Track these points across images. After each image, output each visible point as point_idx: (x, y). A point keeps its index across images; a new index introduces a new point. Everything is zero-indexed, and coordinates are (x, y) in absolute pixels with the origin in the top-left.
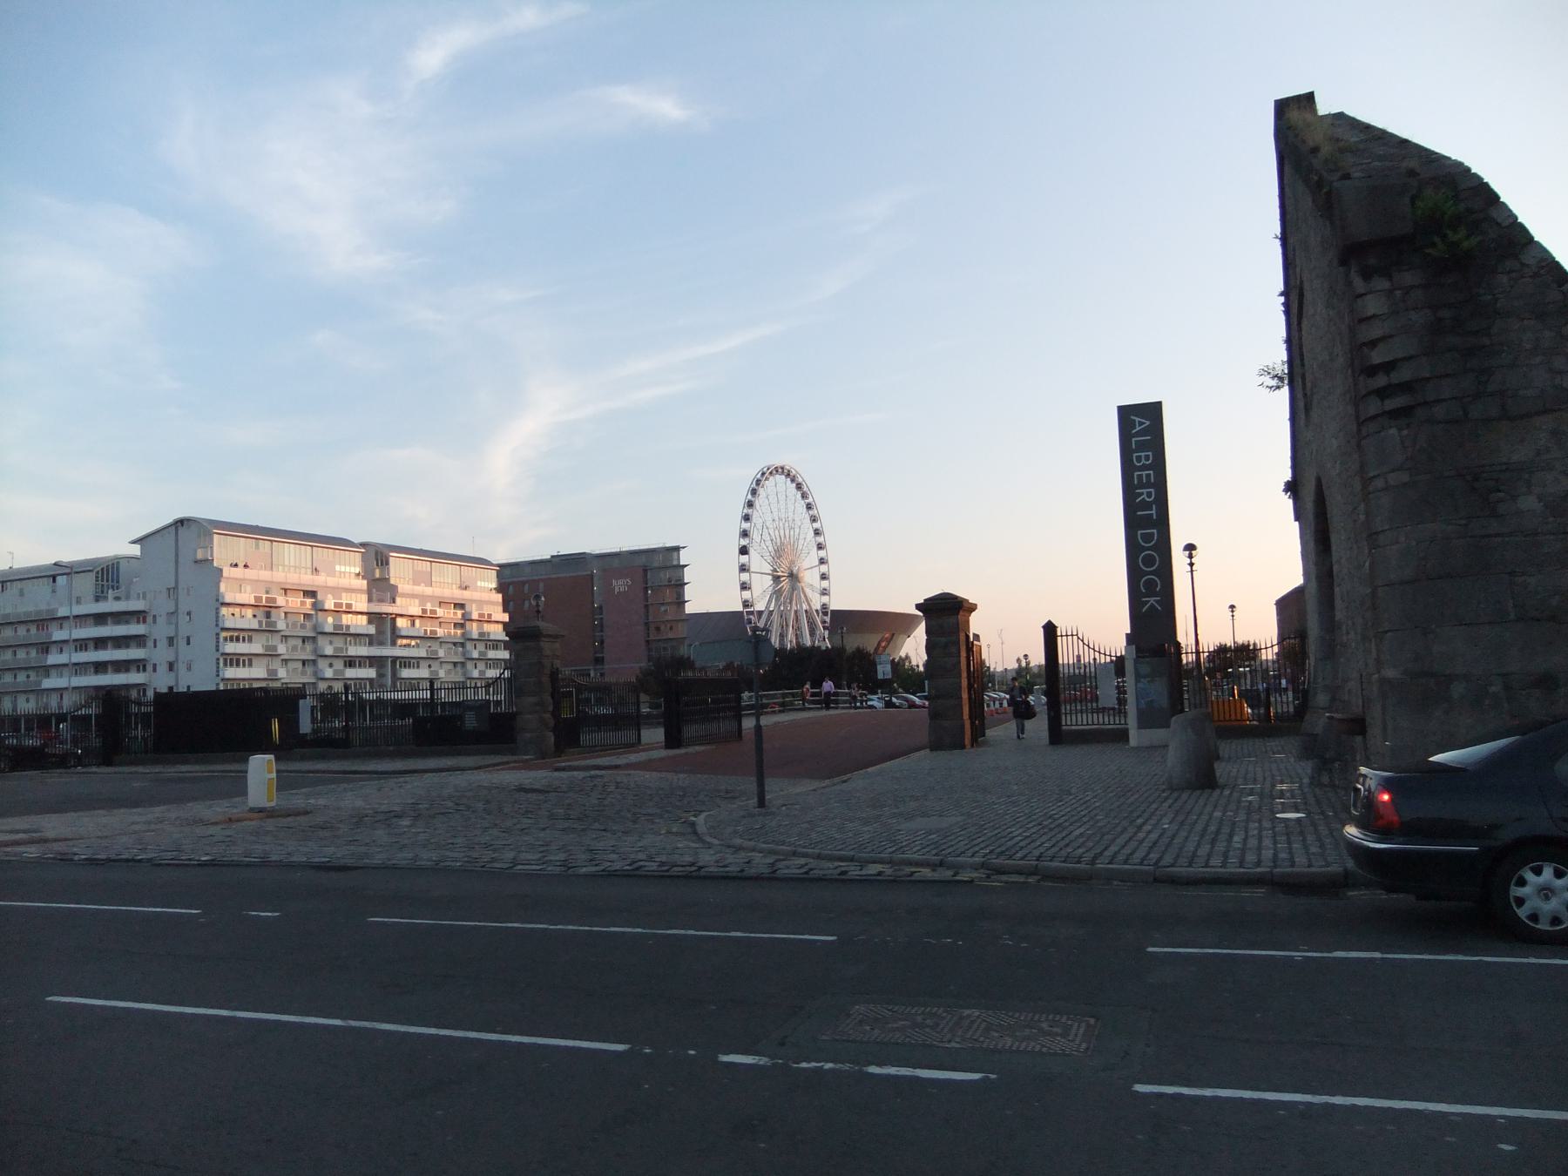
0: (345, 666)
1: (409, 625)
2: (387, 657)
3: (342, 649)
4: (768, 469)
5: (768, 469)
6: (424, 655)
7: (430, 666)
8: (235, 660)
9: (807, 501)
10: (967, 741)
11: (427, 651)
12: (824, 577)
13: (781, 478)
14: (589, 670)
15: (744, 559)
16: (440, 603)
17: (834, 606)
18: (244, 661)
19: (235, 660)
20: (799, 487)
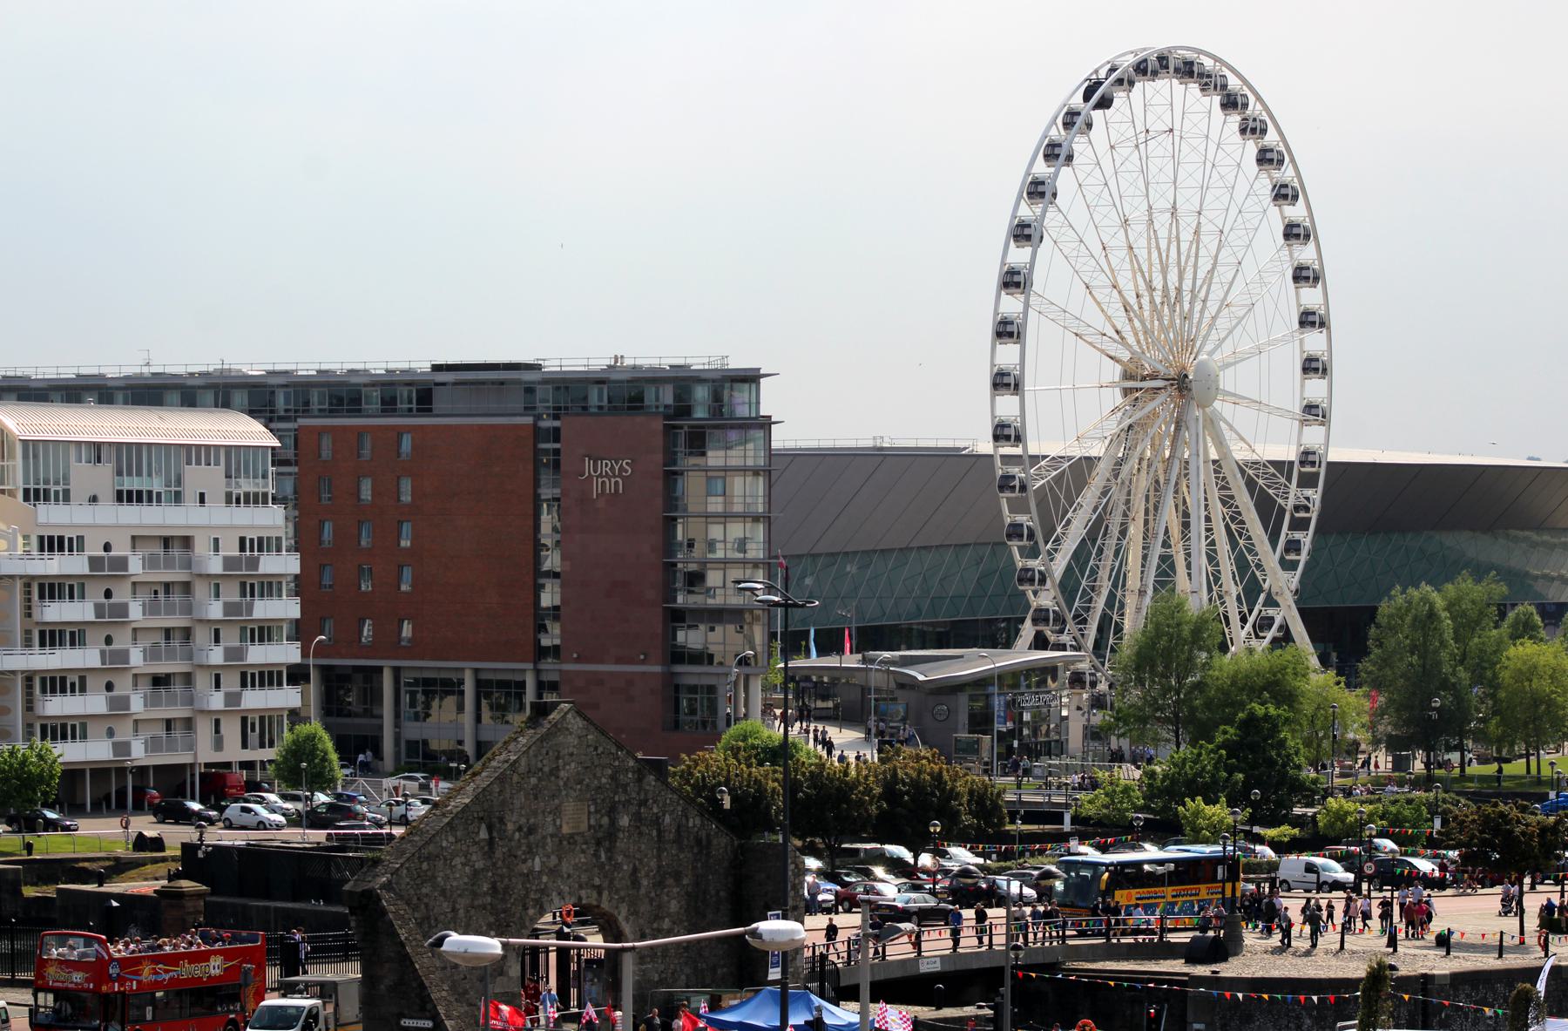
0: (244, 685)
1: (726, 393)
2: (13, 672)
3: (239, 605)
4: (1113, 70)
5: (1113, 70)
6: (97, 663)
7: (109, 687)
8: (61, 730)
9: (1276, 174)
10: (374, 721)
11: (103, 653)
12: (1312, 366)
13: (1164, 88)
14: (524, 671)
15: (1008, 354)
16: (134, 538)
17: (1339, 453)
18: (71, 587)
19: (61, 730)
20: (1231, 103)
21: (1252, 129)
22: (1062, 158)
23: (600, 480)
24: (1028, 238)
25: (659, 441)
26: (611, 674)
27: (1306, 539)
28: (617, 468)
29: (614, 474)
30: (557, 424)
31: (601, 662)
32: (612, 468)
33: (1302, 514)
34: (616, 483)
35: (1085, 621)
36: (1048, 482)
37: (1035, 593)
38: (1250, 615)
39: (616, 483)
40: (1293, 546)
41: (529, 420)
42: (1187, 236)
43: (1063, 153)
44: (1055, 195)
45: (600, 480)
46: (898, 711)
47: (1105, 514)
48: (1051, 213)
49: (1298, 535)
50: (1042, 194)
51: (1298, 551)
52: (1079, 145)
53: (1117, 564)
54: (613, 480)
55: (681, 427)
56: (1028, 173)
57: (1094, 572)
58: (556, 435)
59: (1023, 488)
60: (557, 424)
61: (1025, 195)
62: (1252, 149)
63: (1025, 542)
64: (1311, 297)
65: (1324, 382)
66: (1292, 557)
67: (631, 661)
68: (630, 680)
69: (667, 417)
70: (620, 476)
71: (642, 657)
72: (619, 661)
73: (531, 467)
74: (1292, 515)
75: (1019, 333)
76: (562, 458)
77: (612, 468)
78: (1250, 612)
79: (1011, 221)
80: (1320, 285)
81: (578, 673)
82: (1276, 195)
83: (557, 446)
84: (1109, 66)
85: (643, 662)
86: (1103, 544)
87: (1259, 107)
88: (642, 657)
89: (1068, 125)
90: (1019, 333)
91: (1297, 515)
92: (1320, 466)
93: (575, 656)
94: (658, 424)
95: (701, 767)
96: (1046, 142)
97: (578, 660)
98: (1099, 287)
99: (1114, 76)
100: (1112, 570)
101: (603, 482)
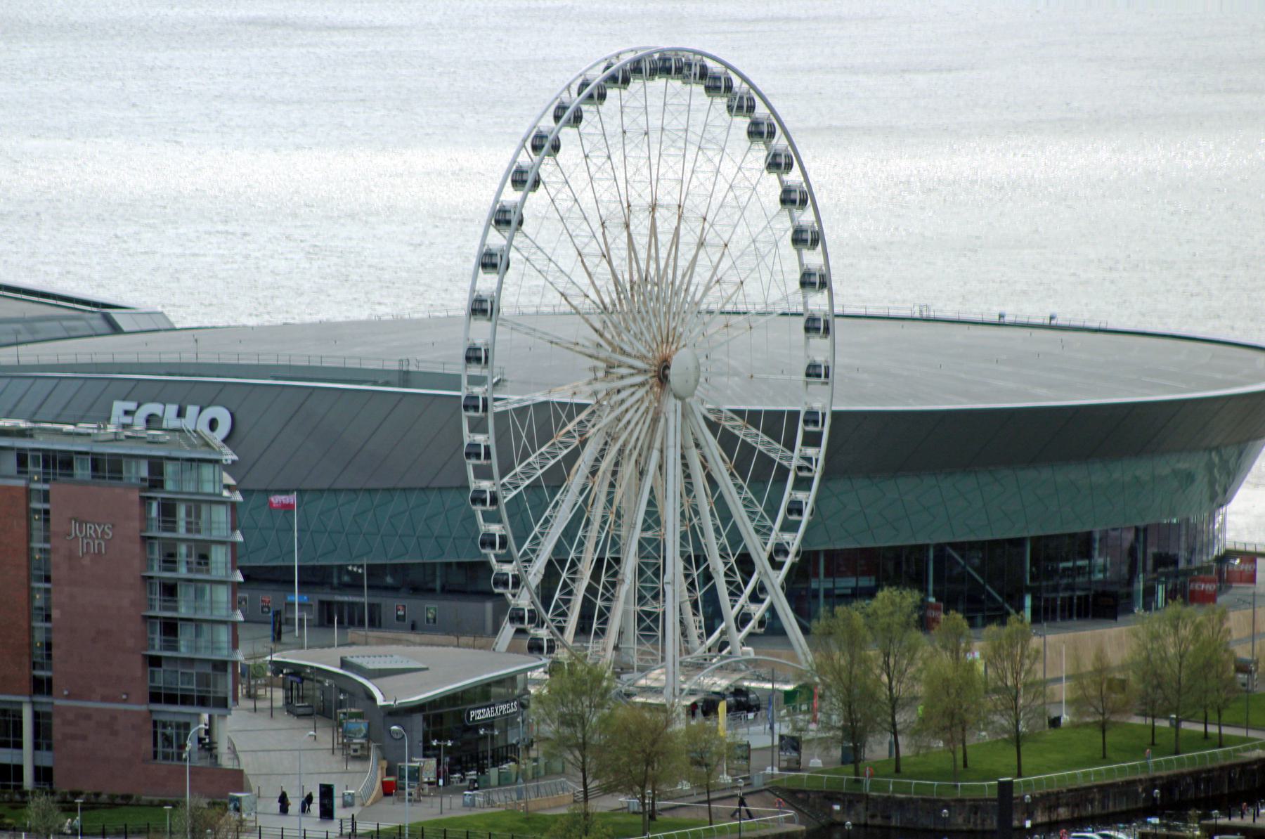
14: (21, 703)
21: (743, 106)
22: (514, 224)
23: (85, 541)
24: (494, 266)
25: (136, 510)
26: (97, 710)
27: (808, 498)
28: (99, 531)
29: (97, 535)
30: (46, 487)
31: (89, 699)
32: (95, 531)
33: (804, 474)
34: (99, 544)
35: (564, 614)
36: (534, 452)
37: (514, 596)
38: (745, 587)
39: (99, 544)
40: (795, 508)
41: (21, 483)
42: (665, 238)
43: (530, 179)
44: (521, 223)
45: (85, 541)
46: (360, 730)
47: (587, 506)
48: (518, 239)
49: (800, 496)
50: (524, 182)
51: (800, 512)
52: (547, 170)
53: (603, 535)
54: (96, 542)
55: (155, 498)
56: (514, 161)
57: (581, 543)
58: (46, 496)
59: (494, 500)
60: (46, 487)
61: (528, 145)
62: (743, 123)
63: (498, 551)
64: (813, 258)
65: (826, 342)
66: (794, 517)
67: (114, 699)
68: (114, 716)
69: (143, 489)
70: (102, 538)
71: (124, 697)
72: (104, 699)
73: (23, 523)
74: (796, 475)
75: (487, 358)
76: (52, 516)
77: (95, 531)
78: (746, 584)
79: (494, 205)
80: (819, 247)
81: (70, 708)
82: (769, 164)
83: (46, 506)
84: (579, 81)
85: (125, 701)
86: (585, 537)
87: (745, 86)
88: (124, 697)
89: (536, 148)
90: (487, 358)
91: (801, 474)
92: (823, 425)
93: (66, 693)
94: (135, 496)
95: (264, 263)
96: (514, 168)
97: (68, 697)
98: (589, 255)
99: (586, 91)
100: (597, 544)
101: (88, 543)
